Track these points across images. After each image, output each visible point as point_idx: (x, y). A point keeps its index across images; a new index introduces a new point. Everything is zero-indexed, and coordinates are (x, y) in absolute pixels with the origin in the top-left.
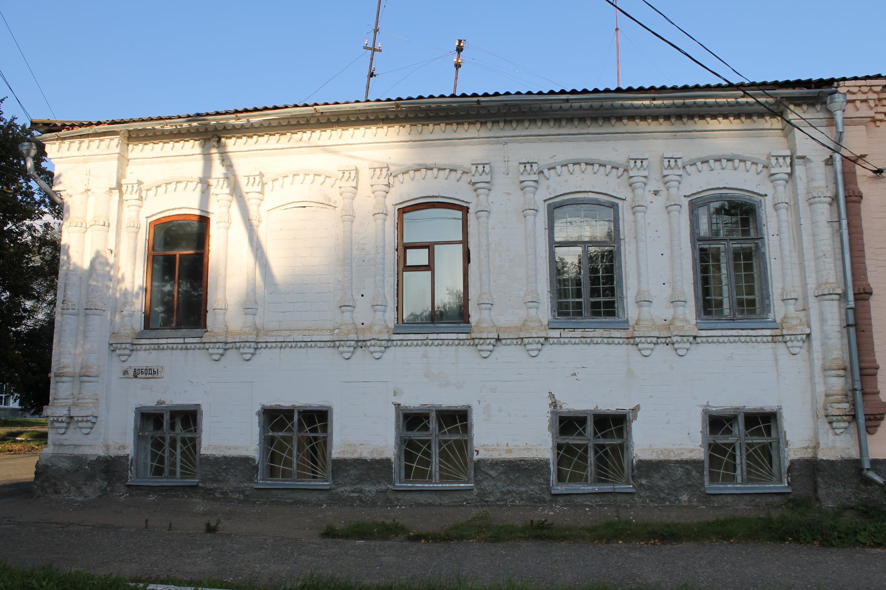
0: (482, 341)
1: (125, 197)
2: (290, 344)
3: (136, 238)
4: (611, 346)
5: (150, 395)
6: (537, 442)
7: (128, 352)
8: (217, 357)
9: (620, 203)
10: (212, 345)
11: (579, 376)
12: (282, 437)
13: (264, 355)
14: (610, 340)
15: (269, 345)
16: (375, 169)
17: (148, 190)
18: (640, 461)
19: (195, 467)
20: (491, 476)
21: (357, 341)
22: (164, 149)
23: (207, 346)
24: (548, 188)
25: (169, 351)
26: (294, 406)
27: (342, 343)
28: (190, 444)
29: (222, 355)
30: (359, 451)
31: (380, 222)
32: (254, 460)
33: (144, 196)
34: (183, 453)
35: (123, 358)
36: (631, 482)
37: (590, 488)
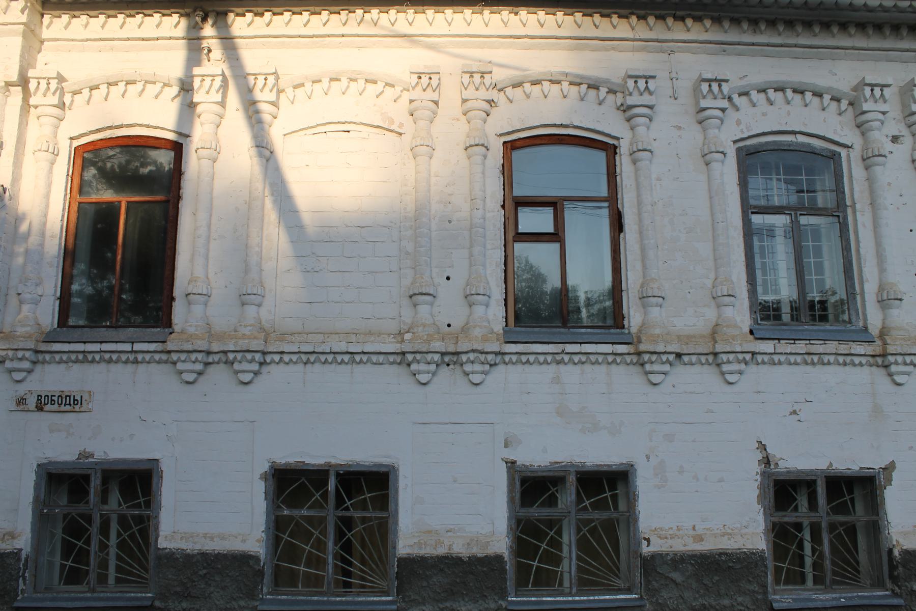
0: (654, 358)
1: (33, 101)
2: (323, 358)
3: (50, 171)
4: (847, 368)
5: (64, 442)
6: (739, 522)
7: (26, 365)
8: (191, 377)
9: (844, 152)
10: (183, 356)
11: (802, 415)
12: (302, 517)
13: (276, 374)
14: (848, 359)
15: (286, 358)
16: (471, 74)
17: (75, 93)
18: (906, 553)
19: (147, 571)
20: (674, 581)
21: (443, 354)
22: (107, 26)
23: (174, 357)
24: (738, 123)
25: (103, 366)
26: (329, 464)
27: (418, 356)
28: (135, 529)
29: (200, 373)
30: (447, 543)
31: (479, 159)
32: (256, 559)
33: (67, 104)
34: (121, 545)
35: (18, 376)
36: (889, 584)
37: (828, 596)
